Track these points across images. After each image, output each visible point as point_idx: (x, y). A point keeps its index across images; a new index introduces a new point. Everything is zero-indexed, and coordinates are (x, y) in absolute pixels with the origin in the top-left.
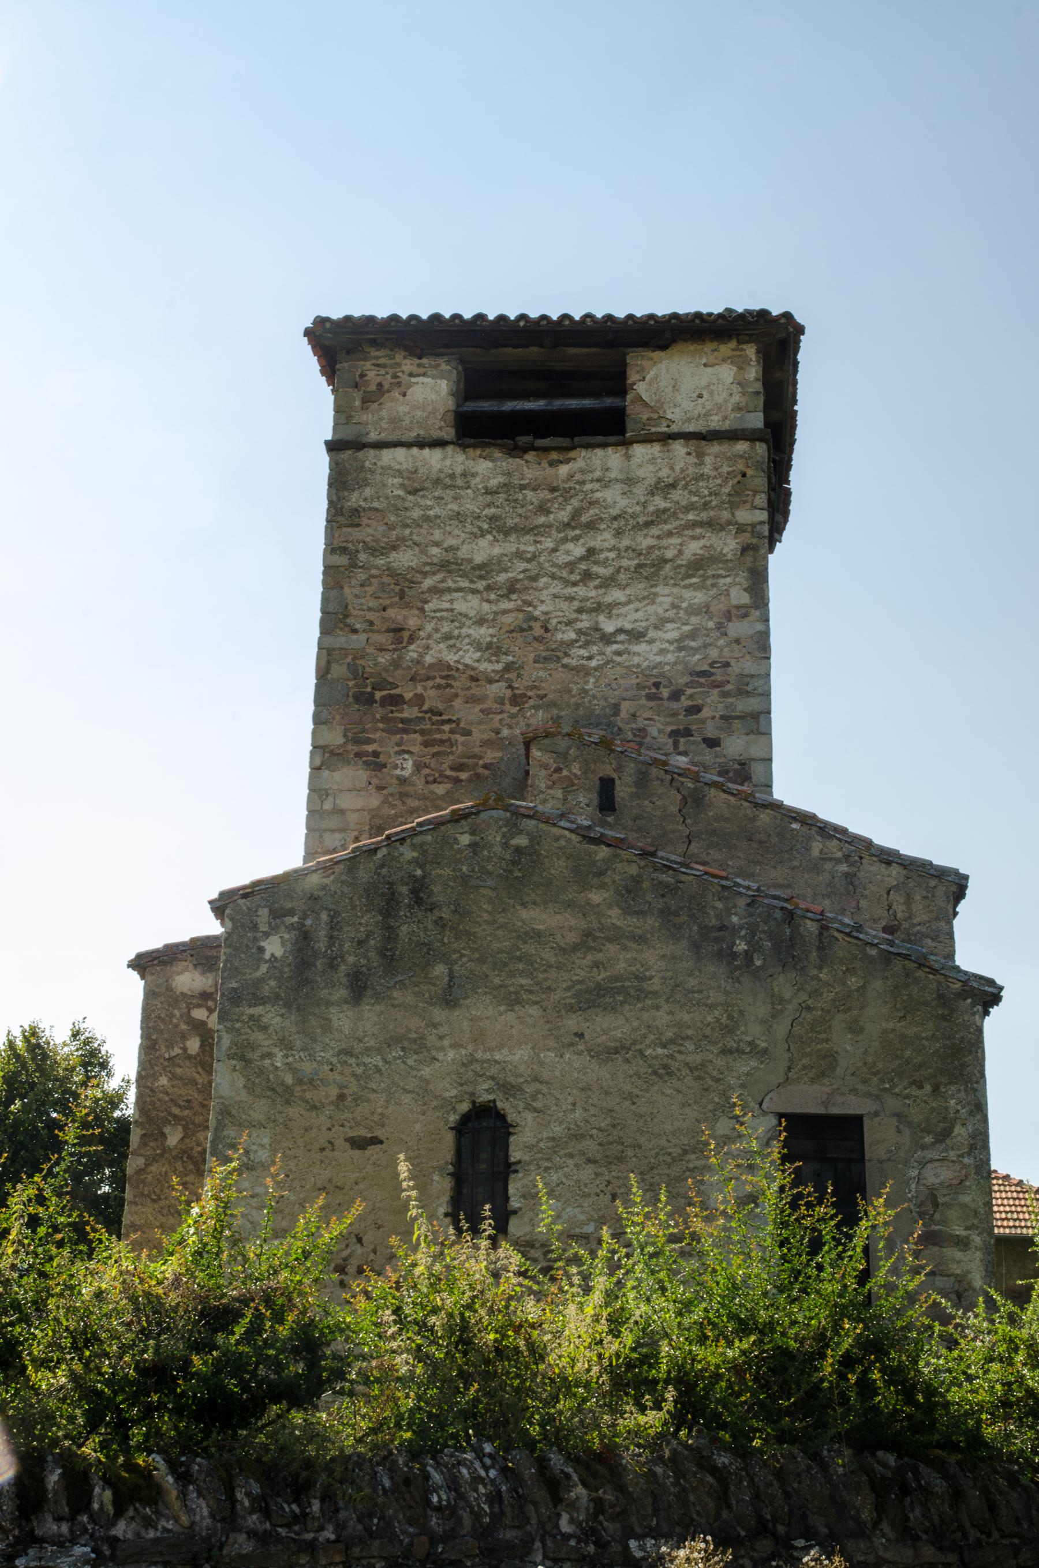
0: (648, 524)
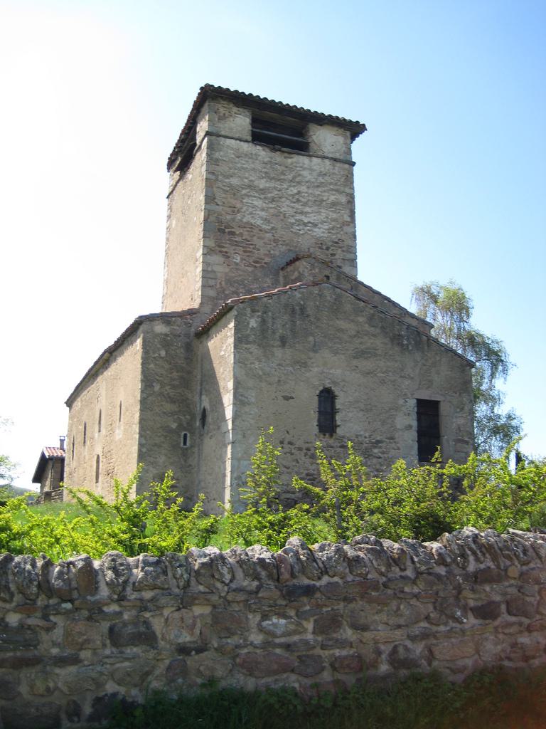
0: (318, 186)
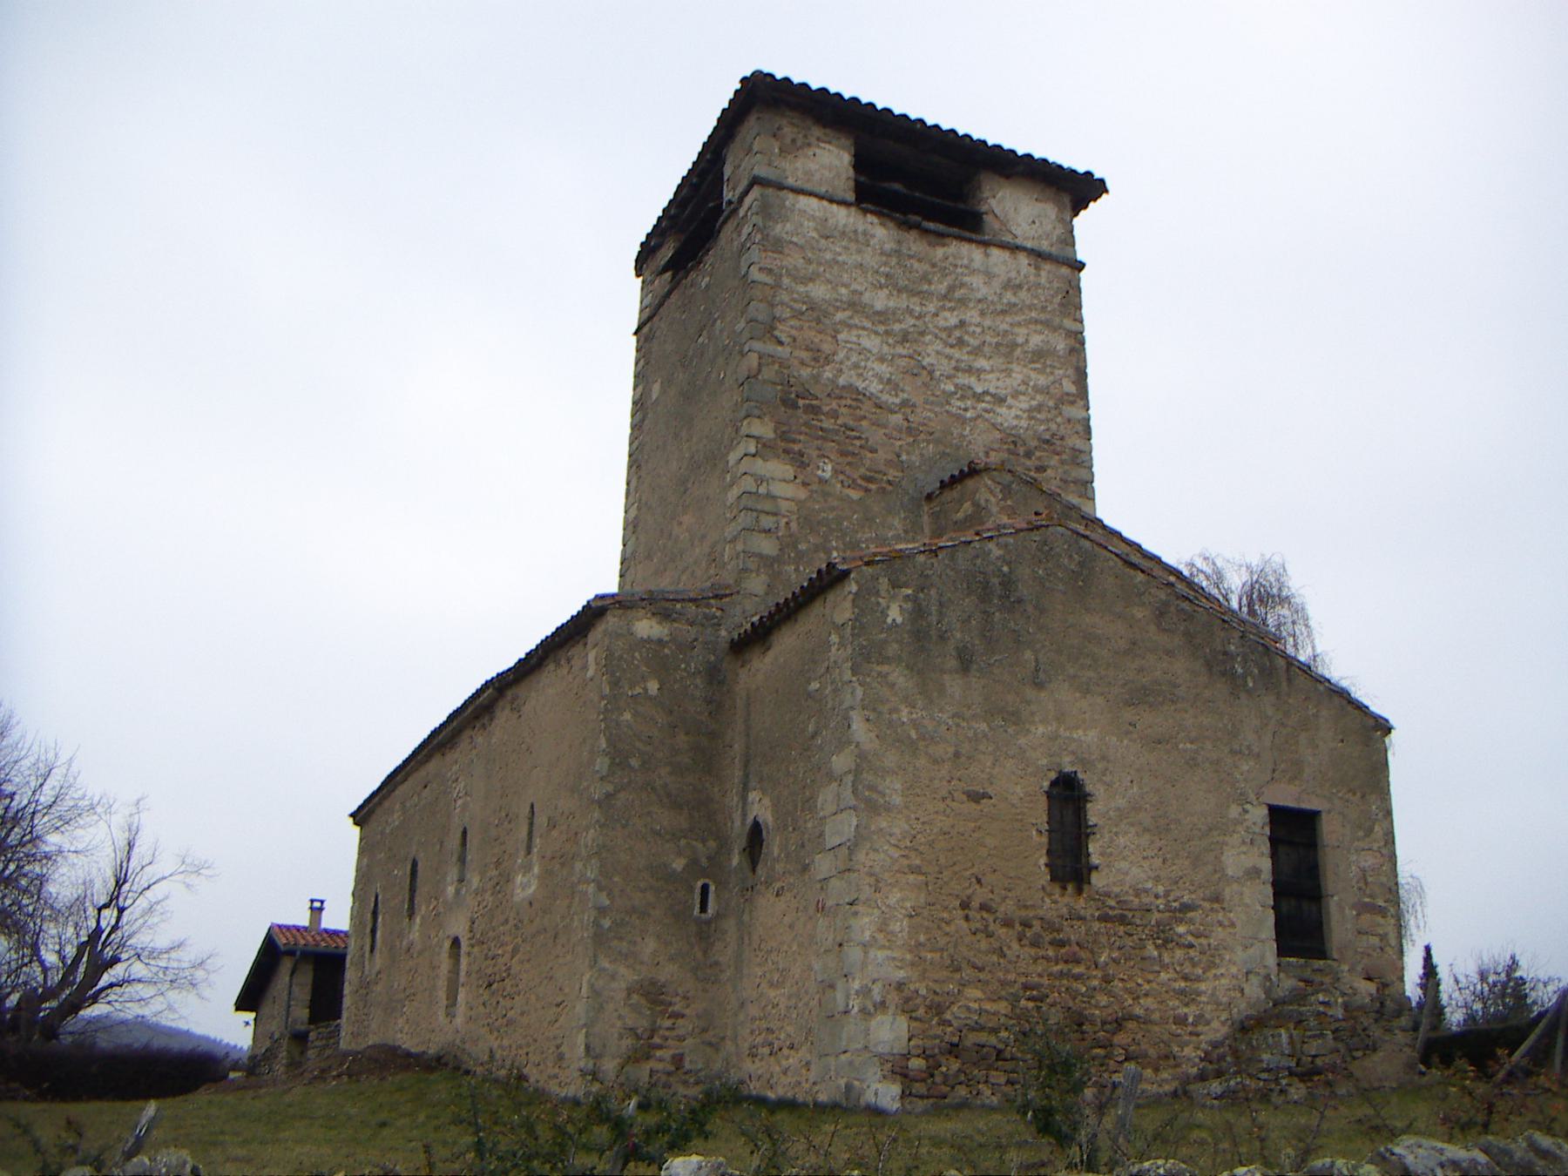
0: (1003, 312)
